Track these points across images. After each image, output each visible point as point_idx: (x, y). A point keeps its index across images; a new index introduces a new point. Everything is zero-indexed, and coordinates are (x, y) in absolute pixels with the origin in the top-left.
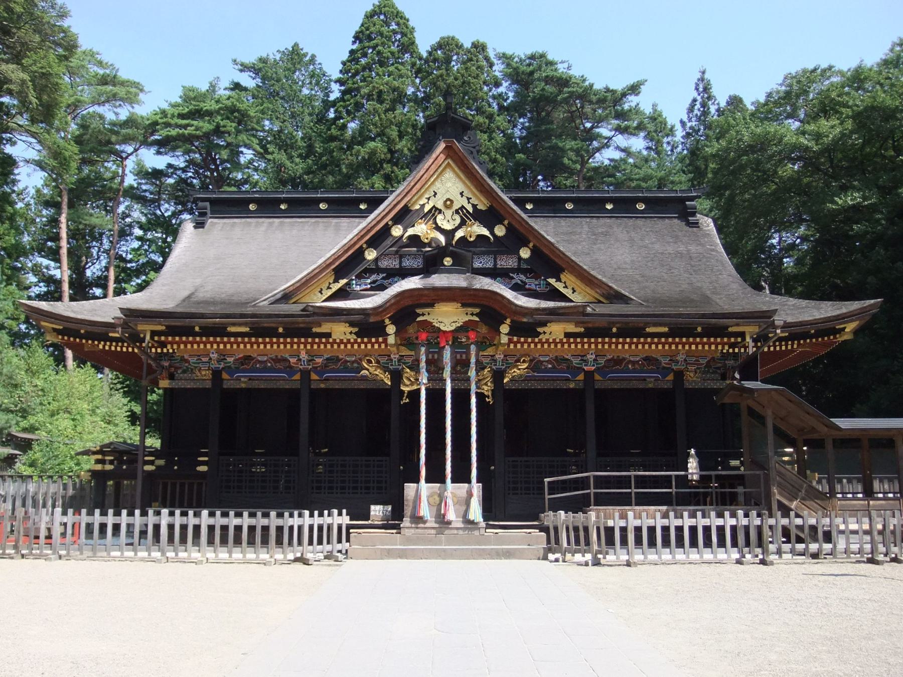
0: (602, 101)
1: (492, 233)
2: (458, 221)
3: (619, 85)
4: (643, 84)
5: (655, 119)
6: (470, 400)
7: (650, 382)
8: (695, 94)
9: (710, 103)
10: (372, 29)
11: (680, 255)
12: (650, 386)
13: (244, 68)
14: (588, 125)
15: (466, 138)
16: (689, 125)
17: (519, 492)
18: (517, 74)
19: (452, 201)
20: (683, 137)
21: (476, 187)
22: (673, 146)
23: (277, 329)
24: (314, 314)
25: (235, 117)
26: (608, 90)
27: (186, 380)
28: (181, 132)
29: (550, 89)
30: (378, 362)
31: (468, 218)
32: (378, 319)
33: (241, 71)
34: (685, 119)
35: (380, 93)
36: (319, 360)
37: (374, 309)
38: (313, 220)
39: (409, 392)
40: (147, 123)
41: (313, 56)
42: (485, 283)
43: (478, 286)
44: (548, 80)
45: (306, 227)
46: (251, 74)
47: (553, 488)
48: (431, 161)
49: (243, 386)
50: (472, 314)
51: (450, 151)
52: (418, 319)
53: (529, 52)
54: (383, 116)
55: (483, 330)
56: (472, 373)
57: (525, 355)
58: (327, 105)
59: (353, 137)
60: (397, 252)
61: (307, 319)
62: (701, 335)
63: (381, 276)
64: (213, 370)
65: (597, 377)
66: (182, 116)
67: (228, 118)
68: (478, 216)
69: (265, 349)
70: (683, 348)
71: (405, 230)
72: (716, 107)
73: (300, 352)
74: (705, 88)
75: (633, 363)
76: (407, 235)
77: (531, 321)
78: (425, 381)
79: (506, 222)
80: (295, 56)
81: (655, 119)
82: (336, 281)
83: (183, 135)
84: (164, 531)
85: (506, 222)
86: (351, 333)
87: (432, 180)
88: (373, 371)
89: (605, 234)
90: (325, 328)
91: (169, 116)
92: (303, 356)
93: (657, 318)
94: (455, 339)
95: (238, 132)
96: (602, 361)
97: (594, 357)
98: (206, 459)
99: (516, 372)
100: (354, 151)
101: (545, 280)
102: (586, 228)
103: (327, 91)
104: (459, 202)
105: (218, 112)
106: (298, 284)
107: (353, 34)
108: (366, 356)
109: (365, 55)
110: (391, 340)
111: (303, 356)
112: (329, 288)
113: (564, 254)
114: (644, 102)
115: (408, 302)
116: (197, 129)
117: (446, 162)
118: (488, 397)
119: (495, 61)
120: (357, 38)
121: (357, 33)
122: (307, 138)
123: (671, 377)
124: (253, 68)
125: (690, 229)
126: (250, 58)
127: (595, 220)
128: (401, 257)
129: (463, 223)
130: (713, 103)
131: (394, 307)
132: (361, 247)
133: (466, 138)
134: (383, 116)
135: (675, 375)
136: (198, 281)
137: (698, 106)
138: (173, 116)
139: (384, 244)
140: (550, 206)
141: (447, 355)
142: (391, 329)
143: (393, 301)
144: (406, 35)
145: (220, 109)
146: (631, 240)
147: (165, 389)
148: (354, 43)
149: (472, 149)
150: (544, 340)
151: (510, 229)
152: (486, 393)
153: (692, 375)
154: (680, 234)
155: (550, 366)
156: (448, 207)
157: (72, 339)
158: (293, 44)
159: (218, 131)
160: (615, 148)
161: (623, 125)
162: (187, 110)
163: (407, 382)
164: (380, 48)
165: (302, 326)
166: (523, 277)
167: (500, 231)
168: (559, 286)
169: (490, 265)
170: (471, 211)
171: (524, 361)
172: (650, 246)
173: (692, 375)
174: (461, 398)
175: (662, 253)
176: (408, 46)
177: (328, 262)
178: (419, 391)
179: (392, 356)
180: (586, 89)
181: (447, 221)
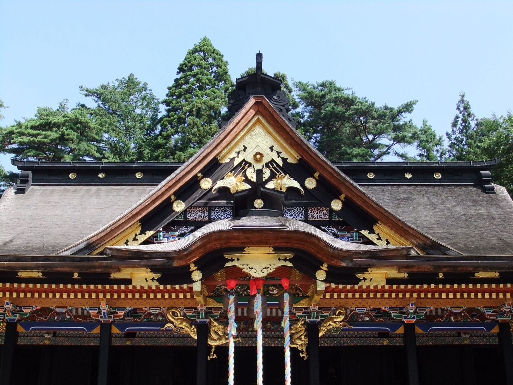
0: (381, 117)
1: (303, 185)
3: (396, 105)
4: (415, 104)
5: (426, 132)
6: (284, 354)
7: (466, 339)
8: (457, 113)
9: (470, 119)
10: (193, 62)
11: (482, 217)
12: (466, 342)
13: (89, 93)
14: (371, 137)
15: (275, 97)
16: (453, 136)
18: (312, 97)
19: (262, 155)
20: (450, 146)
21: (286, 141)
22: (441, 153)
23: (72, 274)
24: (112, 257)
25: (78, 128)
26: (387, 108)
28: (31, 139)
29: (340, 109)
31: (278, 171)
32: (182, 263)
33: (86, 95)
34: (450, 132)
35: (199, 109)
37: (178, 252)
38: (129, 188)
39: (217, 347)
40: (4, 132)
41: (145, 84)
42: (296, 224)
43: (291, 228)
44: (337, 101)
45: (122, 194)
46: (94, 98)
49: (47, 342)
50: (285, 260)
51: (260, 108)
52: (227, 265)
53: (321, 81)
54: (201, 128)
55: (297, 276)
56: (286, 324)
57: (341, 307)
58: (155, 121)
59: (176, 146)
60: (205, 205)
61: (105, 263)
64: (7, 323)
65: (419, 330)
66: (33, 128)
67: (71, 128)
68: (288, 169)
69: (63, 300)
71: (214, 182)
72: (476, 122)
73: (98, 303)
74: (465, 108)
75: (456, 315)
76: (216, 187)
77: (350, 265)
78: (234, 332)
79: (317, 175)
80: (131, 85)
81: (426, 132)
82: (143, 232)
83: (34, 142)
85: (317, 175)
86: (153, 279)
87: (242, 134)
88: (178, 324)
89: (408, 199)
90: (124, 274)
91: (23, 127)
93: (487, 263)
94: (266, 287)
95: (81, 140)
97: (414, 308)
99: (330, 325)
100: (176, 156)
101: (358, 232)
102: (388, 194)
103: (156, 110)
104: (269, 156)
105: (64, 125)
106: (103, 234)
107: (178, 66)
109: (187, 82)
111: (104, 307)
113: (377, 205)
114: (415, 119)
115: (215, 245)
116: (45, 137)
117: (256, 118)
118: (302, 352)
119: (293, 88)
120: (181, 69)
121: (181, 65)
122: (139, 148)
124: (95, 93)
125: (487, 195)
126: (94, 85)
127: (395, 188)
128: (210, 209)
130: (473, 120)
131: (201, 250)
132: (169, 198)
133: (275, 97)
134: (201, 128)
137: (460, 121)
138: (27, 128)
139: (193, 196)
141: (258, 303)
142: (197, 276)
143: (199, 244)
144: (221, 67)
145: (66, 121)
146: (432, 204)
148: (178, 73)
149: (280, 107)
150: (364, 287)
151: (320, 181)
152: (300, 348)
154: (478, 198)
155: (367, 319)
156: (258, 161)
158: (129, 75)
159: (63, 139)
160: (396, 153)
161: (400, 135)
162: (38, 123)
163: (215, 336)
164: (200, 76)
167: (311, 184)
170: (281, 164)
171: (340, 314)
172: (452, 209)
174: (274, 355)
175: (464, 215)
176: (222, 75)
177: (134, 212)
179: (199, 308)
180: (368, 107)
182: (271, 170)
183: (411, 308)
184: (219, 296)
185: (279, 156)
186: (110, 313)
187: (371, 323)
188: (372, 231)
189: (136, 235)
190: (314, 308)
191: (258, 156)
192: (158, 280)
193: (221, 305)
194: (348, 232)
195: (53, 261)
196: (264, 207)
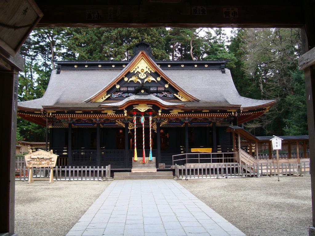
1: (156, 80)
2: (145, 76)
27: (57, 125)
30: (121, 120)
39: (131, 129)
42: (153, 97)
47: (175, 158)
48: (137, 57)
50: (150, 107)
63: (121, 93)
68: (151, 74)
71: (129, 79)
75: (200, 120)
82: (107, 95)
84: (57, 172)
90: (105, 112)
92: (98, 119)
93: (206, 108)
101: (173, 94)
110: (126, 115)
123: (211, 124)
140: (175, 66)
142: (125, 112)
156: (142, 72)
165: (99, 111)
166: (166, 93)
168: (177, 96)
169: (155, 89)
170: (150, 72)
171: (166, 120)
178: (134, 129)
181: (142, 76)
182: (146, 75)
183: (187, 119)
184: (132, 115)
185: (149, 70)
186: (99, 120)
187: (176, 122)
188: (177, 94)
191: (142, 70)
195: (138, 177)
196: (144, 92)
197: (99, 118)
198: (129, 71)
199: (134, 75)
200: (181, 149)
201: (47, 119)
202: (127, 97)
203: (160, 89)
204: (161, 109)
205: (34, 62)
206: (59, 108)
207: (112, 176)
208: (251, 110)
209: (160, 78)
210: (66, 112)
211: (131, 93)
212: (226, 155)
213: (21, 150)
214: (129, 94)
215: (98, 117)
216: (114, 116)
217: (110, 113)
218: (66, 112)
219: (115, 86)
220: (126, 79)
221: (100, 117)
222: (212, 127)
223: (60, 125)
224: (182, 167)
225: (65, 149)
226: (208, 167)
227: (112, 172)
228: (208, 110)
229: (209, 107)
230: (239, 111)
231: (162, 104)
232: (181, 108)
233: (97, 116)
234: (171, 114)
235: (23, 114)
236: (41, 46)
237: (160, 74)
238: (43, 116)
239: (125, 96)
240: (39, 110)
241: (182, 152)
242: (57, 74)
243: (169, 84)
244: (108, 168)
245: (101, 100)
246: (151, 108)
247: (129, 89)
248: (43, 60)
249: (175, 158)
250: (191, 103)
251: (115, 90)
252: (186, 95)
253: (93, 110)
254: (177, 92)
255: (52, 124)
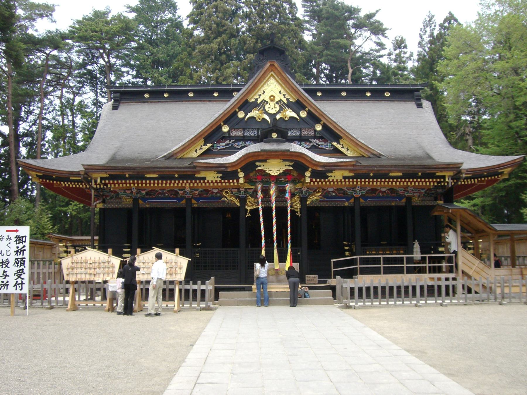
2: (278, 108)
17: (214, 268)
19: (274, 97)
27: (112, 203)
36: (197, 192)
39: (251, 210)
42: (296, 147)
47: (337, 264)
50: (289, 166)
52: (257, 169)
55: (295, 174)
62: (421, 178)
63: (232, 141)
68: (289, 105)
70: (412, 183)
71: (246, 115)
75: (383, 192)
82: (205, 144)
86: (218, 177)
90: (202, 175)
92: (188, 190)
93: (397, 168)
96: (364, 191)
98: (129, 250)
108: (225, 189)
110: (242, 181)
112: (201, 149)
123: (404, 200)
129: (281, 110)
135: (406, 200)
136: (118, 144)
140: (331, 94)
142: (241, 175)
147: (100, 209)
151: (309, 113)
152: (296, 210)
153: (416, 199)
155: (334, 194)
156: (272, 100)
157: (48, 181)
165: (189, 174)
166: (317, 141)
168: (339, 147)
169: (297, 134)
170: (286, 102)
171: (319, 192)
173: (416, 199)
174: (282, 211)
181: (272, 108)
185: (284, 97)
186: (191, 192)
188: (339, 143)
189: (201, 146)
190: (304, 189)
191: (272, 98)
192: (220, 177)
193: (253, 187)
194: (325, 142)
196: (277, 137)
197: (190, 187)
198: (247, 100)
199: (256, 107)
200: (346, 248)
201: (93, 191)
202: (242, 148)
203: (304, 133)
204: (310, 169)
205: (78, 99)
206: (115, 168)
207: (217, 298)
208: (477, 173)
209: (306, 113)
210: (127, 176)
211: (251, 140)
212: (432, 260)
213: (54, 249)
214: (247, 143)
215: (188, 185)
216: (220, 184)
217: (212, 177)
218: (127, 176)
219: (220, 127)
220: (241, 115)
221: (192, 185)
222: (406, 206)
223: (117, 203)
224: (349, 283)
225: (128, 247)
226: (399, 283)
227: (217, 291)
228: (399, 171)
229: (403, 166)
230: (457, 176)
231: (313, 160)
232: (349, 167)
233: (187, 185)
234: (329, 181)
235: (50, 181)
236: (90, 72)
237: (307, 105)
238: (86, 186)
239: (239, 147)
240: (77, 174)
241: (347, 253)
242: (113, 109)
243: (324, 123)
244: (209, 286)
245: (194, 155)
246: (291, 168)
247: (247, 133)
248: (92, 95)
249: (337, 264)
250: (365, 159)
251: (220, 134)
252: (356, 144)
253: (180, 172)
254: (337, 138)
255: (101, 201)
